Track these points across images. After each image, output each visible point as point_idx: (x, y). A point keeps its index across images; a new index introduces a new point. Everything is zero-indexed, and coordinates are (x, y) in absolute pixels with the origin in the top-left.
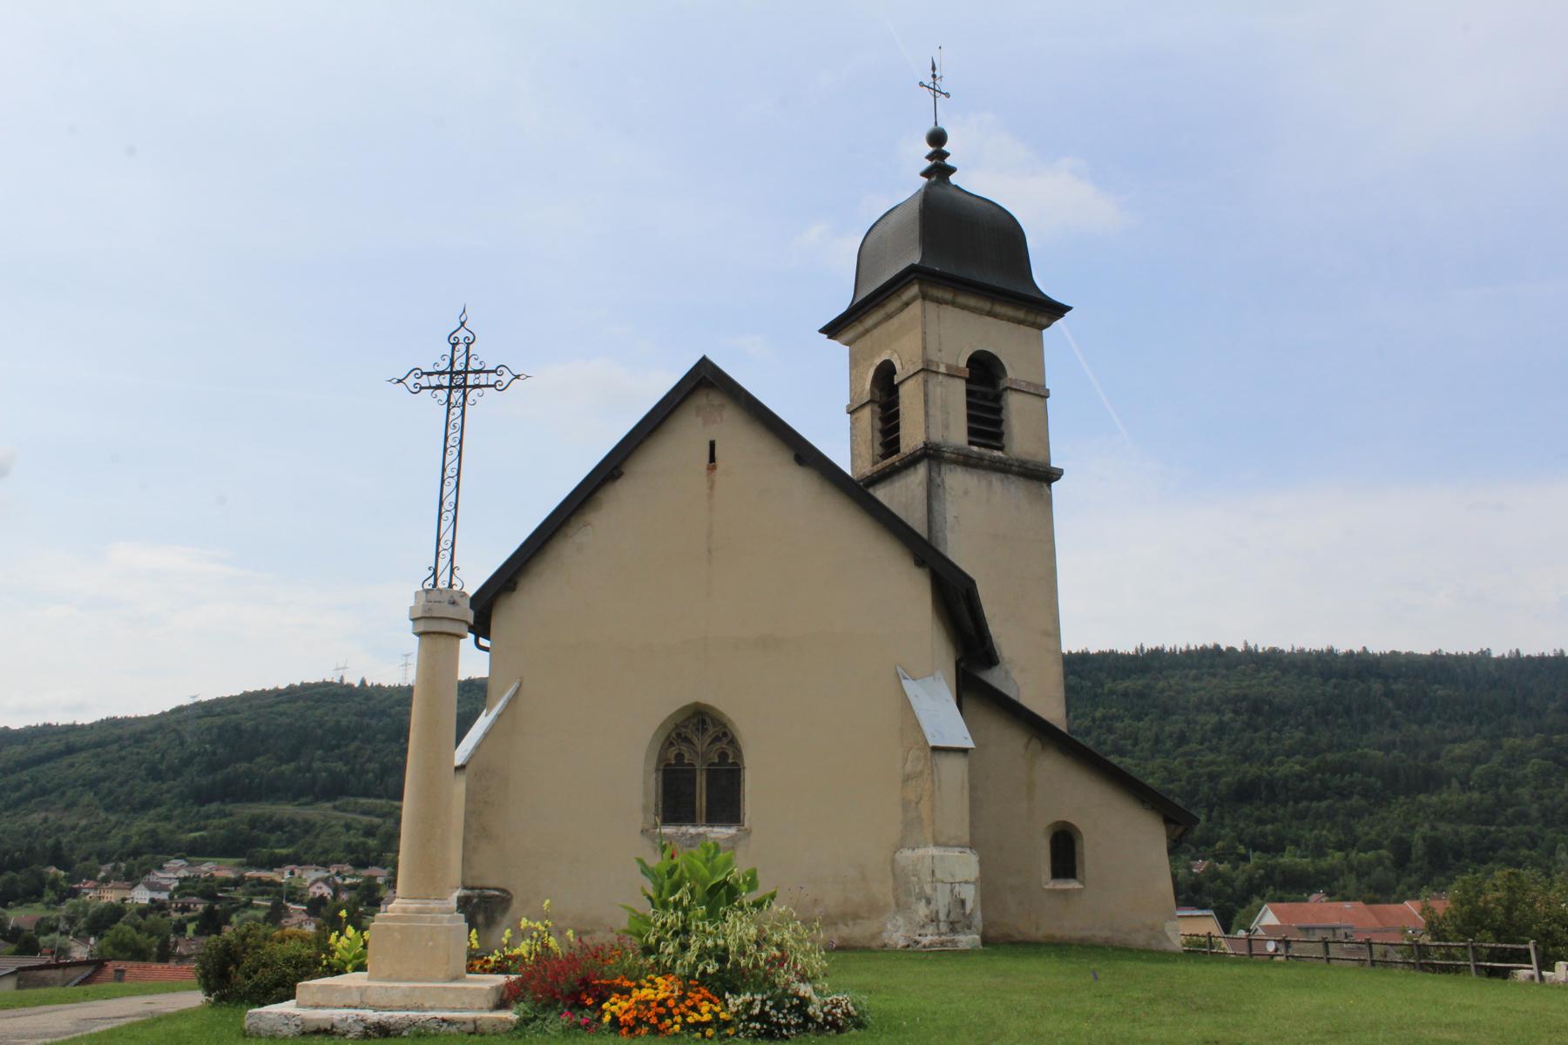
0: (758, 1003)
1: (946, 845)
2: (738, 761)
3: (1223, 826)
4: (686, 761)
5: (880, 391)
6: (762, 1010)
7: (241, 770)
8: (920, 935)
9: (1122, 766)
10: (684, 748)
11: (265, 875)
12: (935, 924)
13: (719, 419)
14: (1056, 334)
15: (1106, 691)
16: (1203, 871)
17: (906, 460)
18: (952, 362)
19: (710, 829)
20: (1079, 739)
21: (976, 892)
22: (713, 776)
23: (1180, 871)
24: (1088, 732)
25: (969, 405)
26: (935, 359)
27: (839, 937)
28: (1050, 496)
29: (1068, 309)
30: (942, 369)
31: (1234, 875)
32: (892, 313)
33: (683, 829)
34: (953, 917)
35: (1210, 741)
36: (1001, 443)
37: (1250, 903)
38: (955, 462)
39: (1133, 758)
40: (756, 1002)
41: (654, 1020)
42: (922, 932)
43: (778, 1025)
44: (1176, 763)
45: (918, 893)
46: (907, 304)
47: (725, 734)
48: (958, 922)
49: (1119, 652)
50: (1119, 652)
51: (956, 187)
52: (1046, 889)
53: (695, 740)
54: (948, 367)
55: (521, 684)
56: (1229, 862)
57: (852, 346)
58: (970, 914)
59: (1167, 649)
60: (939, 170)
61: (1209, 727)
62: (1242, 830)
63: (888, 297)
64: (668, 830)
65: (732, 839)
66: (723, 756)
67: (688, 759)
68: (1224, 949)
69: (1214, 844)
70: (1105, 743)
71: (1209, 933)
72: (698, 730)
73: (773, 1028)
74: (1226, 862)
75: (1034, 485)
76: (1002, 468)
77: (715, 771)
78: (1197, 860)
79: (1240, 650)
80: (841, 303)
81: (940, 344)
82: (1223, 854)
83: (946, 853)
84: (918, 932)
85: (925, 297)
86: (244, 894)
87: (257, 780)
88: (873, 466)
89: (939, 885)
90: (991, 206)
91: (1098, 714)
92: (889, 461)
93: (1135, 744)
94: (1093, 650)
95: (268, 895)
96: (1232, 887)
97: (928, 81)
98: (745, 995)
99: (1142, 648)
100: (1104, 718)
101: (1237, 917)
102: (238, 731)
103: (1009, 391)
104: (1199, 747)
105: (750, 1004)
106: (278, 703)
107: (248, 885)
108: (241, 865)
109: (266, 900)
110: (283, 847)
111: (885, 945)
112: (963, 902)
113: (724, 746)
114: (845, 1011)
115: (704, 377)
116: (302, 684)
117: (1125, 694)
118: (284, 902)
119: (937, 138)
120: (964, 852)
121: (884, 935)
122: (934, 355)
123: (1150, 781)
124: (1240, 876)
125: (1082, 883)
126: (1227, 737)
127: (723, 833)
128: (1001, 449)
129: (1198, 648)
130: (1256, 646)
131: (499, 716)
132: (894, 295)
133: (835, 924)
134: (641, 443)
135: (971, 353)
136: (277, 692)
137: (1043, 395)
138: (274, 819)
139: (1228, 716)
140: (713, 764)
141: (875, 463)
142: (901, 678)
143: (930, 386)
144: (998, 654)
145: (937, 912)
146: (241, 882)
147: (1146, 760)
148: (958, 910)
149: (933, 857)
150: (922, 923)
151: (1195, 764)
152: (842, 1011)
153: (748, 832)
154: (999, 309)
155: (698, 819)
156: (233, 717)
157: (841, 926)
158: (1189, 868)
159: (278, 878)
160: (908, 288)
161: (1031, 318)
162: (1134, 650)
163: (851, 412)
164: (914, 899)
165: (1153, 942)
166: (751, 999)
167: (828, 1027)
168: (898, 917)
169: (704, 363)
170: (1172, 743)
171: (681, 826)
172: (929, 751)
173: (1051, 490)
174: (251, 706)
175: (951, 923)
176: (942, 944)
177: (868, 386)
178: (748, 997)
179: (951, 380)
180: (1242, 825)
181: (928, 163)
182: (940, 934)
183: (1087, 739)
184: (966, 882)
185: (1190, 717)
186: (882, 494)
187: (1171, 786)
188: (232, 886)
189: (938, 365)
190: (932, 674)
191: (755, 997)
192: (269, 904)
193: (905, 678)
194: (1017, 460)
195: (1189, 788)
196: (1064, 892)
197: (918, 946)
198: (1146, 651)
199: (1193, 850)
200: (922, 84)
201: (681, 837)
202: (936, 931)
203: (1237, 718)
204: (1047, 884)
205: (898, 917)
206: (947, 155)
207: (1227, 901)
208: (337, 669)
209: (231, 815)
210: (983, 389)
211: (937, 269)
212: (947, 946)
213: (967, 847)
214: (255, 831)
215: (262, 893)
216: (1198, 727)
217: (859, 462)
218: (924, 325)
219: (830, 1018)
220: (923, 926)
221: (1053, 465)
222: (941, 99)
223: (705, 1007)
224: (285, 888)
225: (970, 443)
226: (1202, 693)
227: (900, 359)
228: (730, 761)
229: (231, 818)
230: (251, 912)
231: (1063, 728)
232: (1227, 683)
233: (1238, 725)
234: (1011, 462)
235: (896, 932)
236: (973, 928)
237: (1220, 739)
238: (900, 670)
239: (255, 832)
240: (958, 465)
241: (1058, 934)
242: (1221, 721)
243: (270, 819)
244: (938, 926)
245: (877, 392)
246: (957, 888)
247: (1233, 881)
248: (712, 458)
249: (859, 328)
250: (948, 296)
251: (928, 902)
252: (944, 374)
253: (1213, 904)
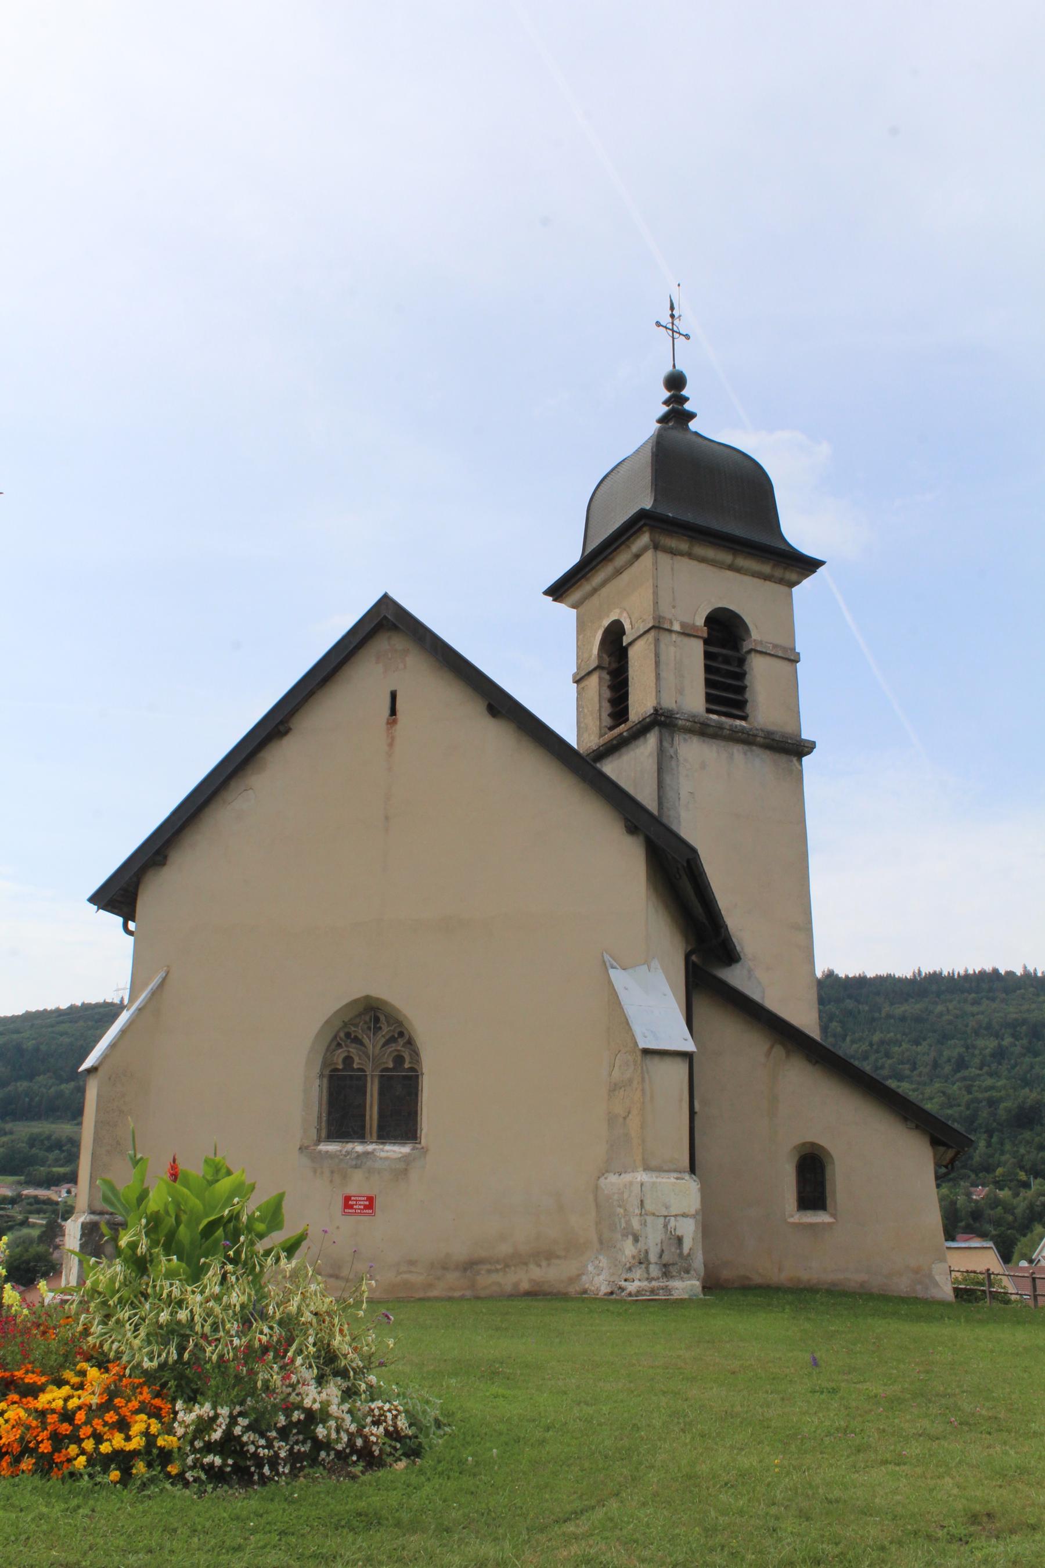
0: (223, 1422)
1: (659, 1169)
2: (416, 1067)
3: (1003, 1153)
4: (355, 1066)
5: (609, 657)
6: (228, 1434)
7: (20, 1089)
8: (626, 1280)
9: (900, 1091)
10: (353, 1050)
11: (42, 1193)
12: (643, 1266)
13: (401, 666)
14: (805, 591)
15: (883, 1015)
16: (983, 1198)
17: (634, 729)
18: (687, 619)
19: (381, 1147)
20: (856, 1063)
21: (696, 1227)
22: (386, 1083)
23: (959, 1197)
24: (865, 1057)
25: (708, 669)
26: (668, 616)
27: (531, 1281)
28: (800, 773)
30: (677, 627)
31: (1015, 1201)
32: (622, 567)
33: (350, 1146)
34: (666, 1258)
35: (989, 1066)
36: (743, 712)
37: (1032, 1231)
38: (690, 731)
39: (911, 1083)
40: (221, 1419)
41: (45, 1447)
42: (629, 1276)
43: (259, 1462)
44: (955, 1087)
45: (624, 1228)
46: (637, 556)
47: (401, 1034)
48: (673, 1264)
49: (897, 976)
50: (897, 976)
51: (696, 434)
52: (789, 1223)
53: (366, 1041)
54: (683, 625)
55: (167, 973)
56: (1010, 1189)
58: (689, 1255)
59: (945, 973)
61: (988, 1051)
62: (1023, 1156)
63: (615, 550)
64: (332, 1147)
65: (406, 1159)
66: (399, 1060)
67: (359, 1063)
68: (1005, 1287)
69: (994, 1171)
70: (882, 1067)
71: (988, 1270)
72: (369, 1028)
73: (248, 1463)
74: (1006, 1189)
75: (783, 759)
76: (747, 739)
77: (391, 1078)
78: (977, 1186)
79: (1019, 974)
80: (571, 556)
81: (674, 600)
82: (1002, 1181)
83: (659, 1180)
84: (624, 1276)
85: (656, 547)
86: (20, 1212)
87: (37, 1099)
88: (600, 738)
89: (649, 1219)
90: (735, 453)
91: (876, 1038)
92: (616, 731)
93: (914, 1068)
94: (870, 974)
95: (45, 1213)
96: (1013, 1214)
97: (666, 320)
98: (202, 1405)
99: (919, 971)
100: (882, 1042)
101: (1019, 1245)
102: (19, 1049)
103: (753, 654)
104: (978, 1072)
105: (205, 1425)
106: (59, 1023)
107: (24, 1202)
108: (19, 1183)
109: (43, 1218)
110: (62, 1166)
111: (585, 1292)
112: (680, 1240)
113: (399, 1048)
114: (391, 1429)
115: (385, 617)
116: (83, 1004)
117: (903, 1019)
118: (59, 1221)
119: (675, 382)
120: (683, 1179)
121: (584, 1278)
122: (666, 611)
123: (928, 1106)
124: (1022, 1202)
125: (834, 1216)
126: (1006, 1061)
127: (394, 1151)
128: (744, 718)
129: (977, 972)
130: (1035, 970)
131: (140, 1010)
132: (623, 547)
133: (526, 1264)
134: (311, 694)
135: (710, 610)
136: (58, 1012)
138: (53, 1137)
139: (1007, 1041)
140: (387, 1069)
141: (601, 736)
142: (609, 967)
143: (662, 646)
144: (738, 948)
145: (647, 1252)
146: (18, 1200)
147: (925, 1084)
148: (673, 1250)
149: (642, 1185)
150: (628, 1265)
151: (975, 1088)
152: (386, 1430)
153: (425, 1151)
154: (741, 562)
155: (368, 1135)
156: (15, 1036)
157: (532, 1266)
158: (969, 1195)
159: (55, 1197)
160: (638, 537)
161: (778, 573)
162: (911, 974)
163: (578, 681)
164: (620, 1237)
165: (919, 1287)
166: (212, 1413)
167: (354, 1458)
168: (601, 1257)
169: (386, 600)
170: (950, 1068)
171: (347, 1142)
172: (639, 1053)
173: (801, 765)
174: (32, 1026)
175: (665, 1265)
176: (653, 1291)
177: (595, 651)
178: (204, 1410)
179: (686, 640)
180: (1022, 1151)
181: (665, 409)
182: (650, 1279)
183: (865, 1064)
184: (684, 1215)
185: (969, 1041)
186: (609, 768)
187: (950, 1112)
188: (9, 1204)
189: (671, 623)
190: (647, 962)
191: (219, 1411)
192: (44, 1222)
193: (613, 967)
194: (762, 730)
195: (968, 1112)
196: (812, 1226)
197: (623, 1294)
198: (923, 974)
199: (973, 1176)
200: (658, 324)
201: (345, 1156)
202: (646, 1275)
203: (1017, 1043)
204: (792, 1216)
205: (601, 1257)
206: (686, 399)
207: (1008, 1229)
208: (118, 990)
209: (11, 1133)
210: (724, 651)
211: (670, 515)
212: (657, 1294)
213: (684, 1172)
214: (34, 1149)
215: (38, 1212)
216: (977, 1052)
217: (586, 735)
218: (655, 578)
219: (359, 1442)
220: (630, 1269)
221: (803, 737)
222: (680, 341)
223: (139, 1424)
224: (61, 1208)
225: (709, 711)
226: (981, 1017)
227: (630, 618)
228: (407, 1066)
229: (10, 1136)
230: (26, 1231)
231: (815, 1033)
232: (1005, 1007)
233: (1017, 1050)
234: (755, 732)
235: (598, 1275)
236: (692, 1272)
237: (1000, 1064)
238: (607, 957)
239: (34, 1151)
240: (695, 735)
241: (805, 1276)
242: (1000, 1046)
243: (49, 1138)
244: (647, 1269)
245: (605, 656)
246: (672, 1222)
247: (1015, 1208)
248: (393, 712)
249: (586, 587)
250: (684, 546)
251: (636, 1239)
252: (678, 633)
253: (994, 1232)
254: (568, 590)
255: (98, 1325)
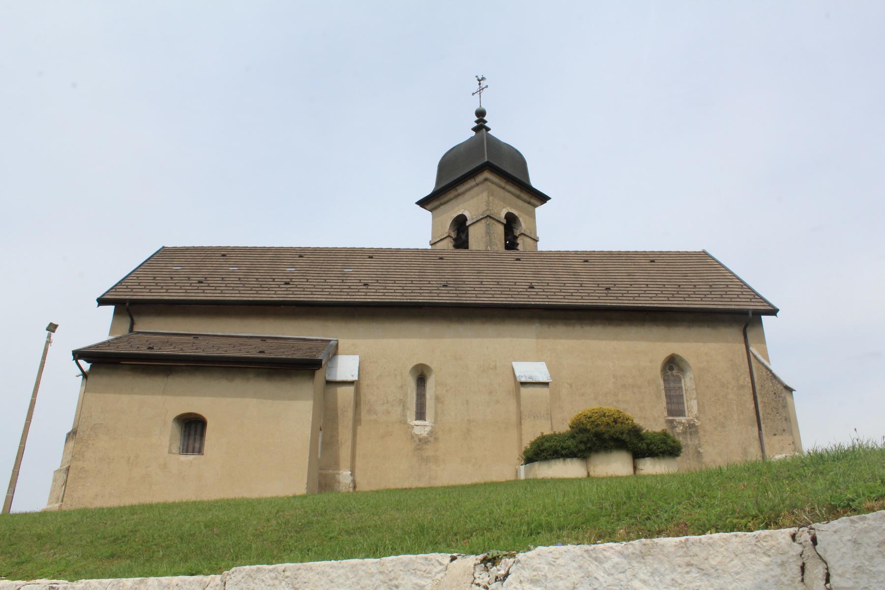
14: (541, 211)
29: (548, 198)
57: (434, 212)
60: (481, 126)
80: (428, 187)
119: (481, 114)
137: (536, 241)
169: (73, 351)
181: (476, 125)
206: (486, 122)
249: (436, 203)
254: (478, 174)
255: (686, 420)
